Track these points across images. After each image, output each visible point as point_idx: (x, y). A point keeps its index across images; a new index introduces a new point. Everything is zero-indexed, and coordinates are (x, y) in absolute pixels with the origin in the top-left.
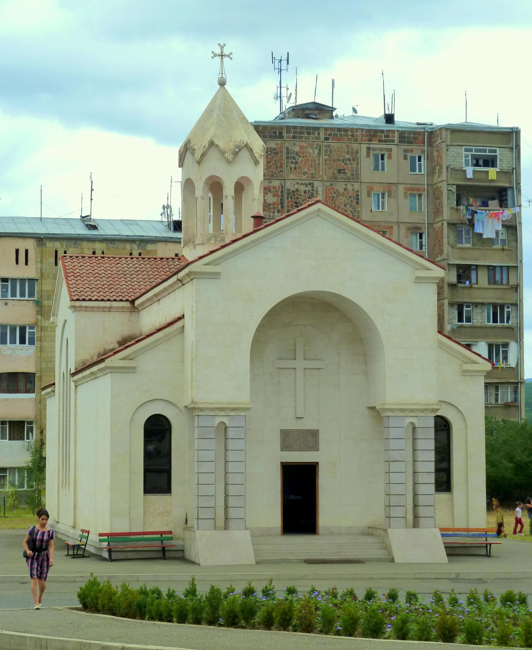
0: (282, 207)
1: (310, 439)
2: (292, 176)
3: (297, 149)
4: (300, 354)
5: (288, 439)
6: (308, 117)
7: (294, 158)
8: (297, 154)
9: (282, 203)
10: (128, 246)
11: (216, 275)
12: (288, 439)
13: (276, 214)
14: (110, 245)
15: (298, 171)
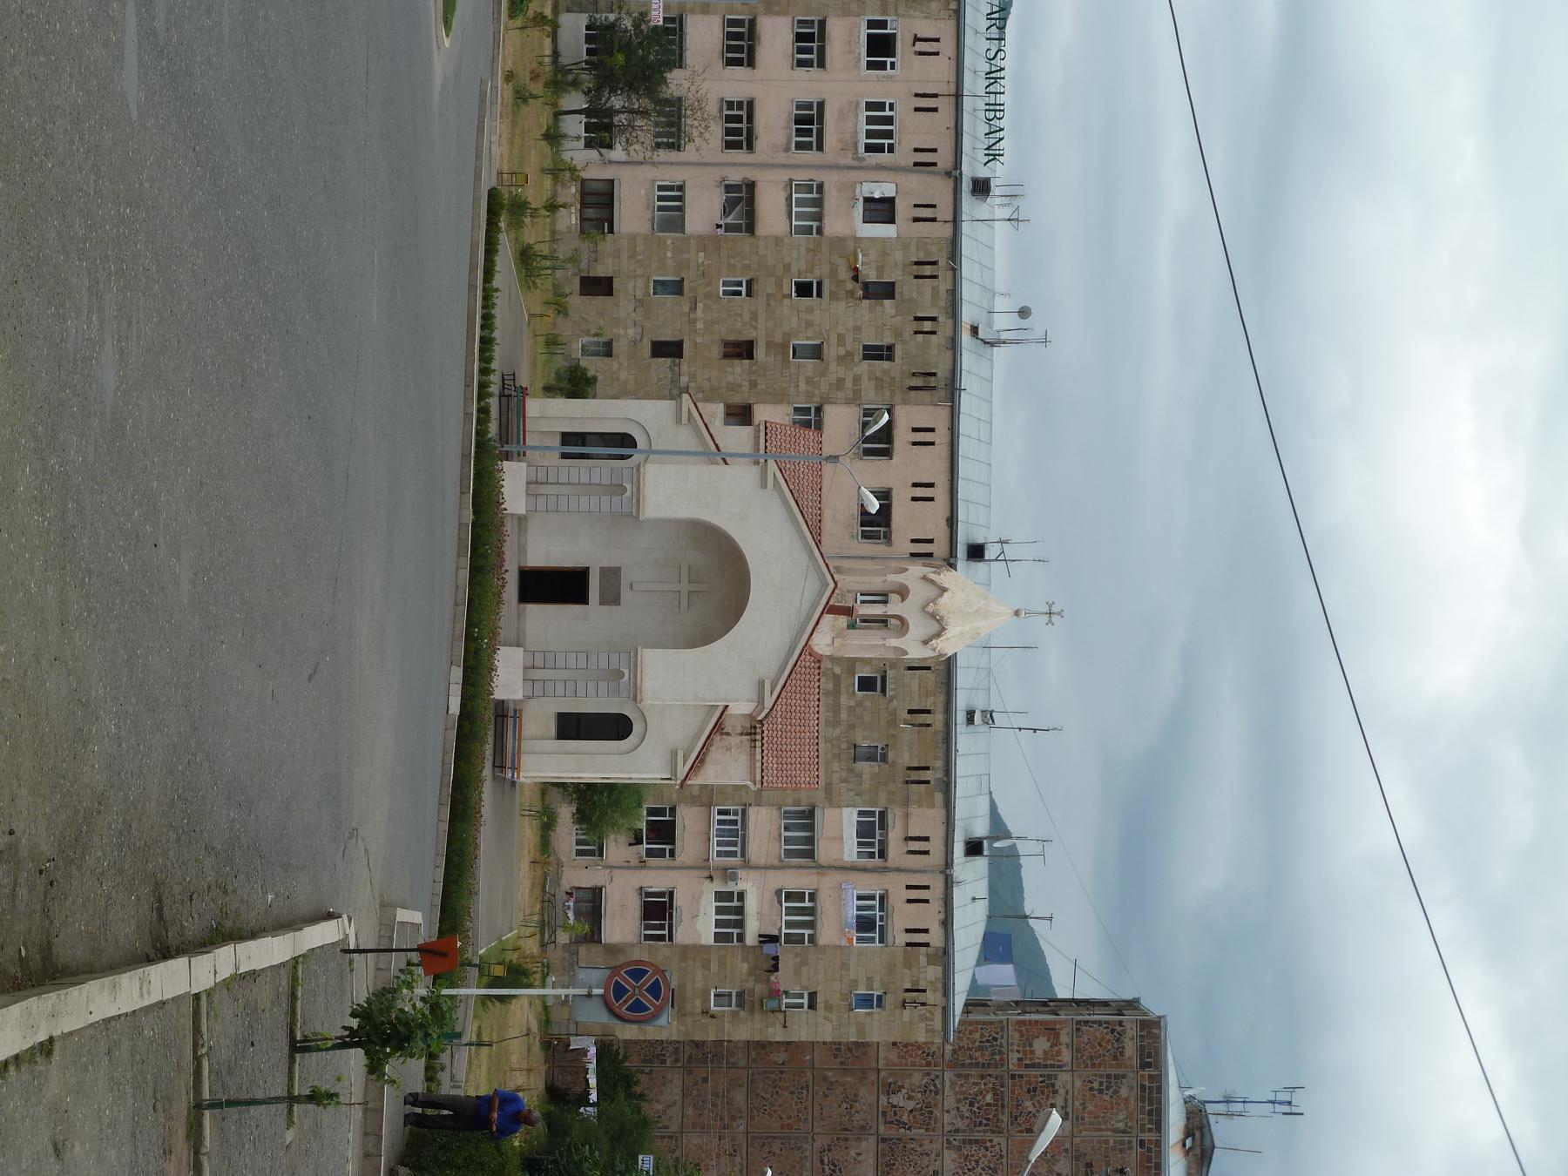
0: (1027, 1066)
1: (611, 597)
2: (1078, 1083)
3: (1124, 1092)
4: (694, 587)
5: (611, 575)
6: (1188, 1133)
7: (1108, 1088)
8: (1116, 1092)
9: (1033, 1066)
10: (939, 764)
11: (764, 485)
12: (611, 575)
13: (1017, 1055)
14: (940, 736)
15: (1088, 1094)
